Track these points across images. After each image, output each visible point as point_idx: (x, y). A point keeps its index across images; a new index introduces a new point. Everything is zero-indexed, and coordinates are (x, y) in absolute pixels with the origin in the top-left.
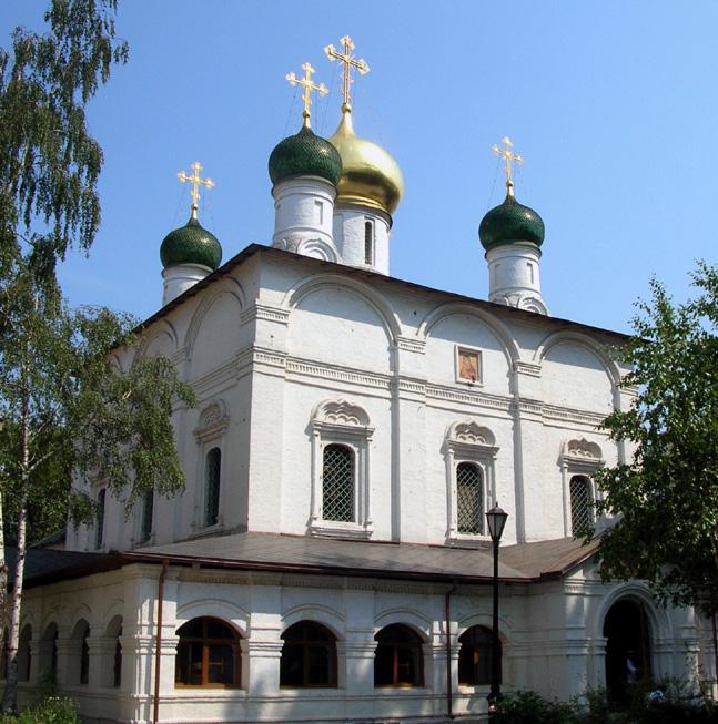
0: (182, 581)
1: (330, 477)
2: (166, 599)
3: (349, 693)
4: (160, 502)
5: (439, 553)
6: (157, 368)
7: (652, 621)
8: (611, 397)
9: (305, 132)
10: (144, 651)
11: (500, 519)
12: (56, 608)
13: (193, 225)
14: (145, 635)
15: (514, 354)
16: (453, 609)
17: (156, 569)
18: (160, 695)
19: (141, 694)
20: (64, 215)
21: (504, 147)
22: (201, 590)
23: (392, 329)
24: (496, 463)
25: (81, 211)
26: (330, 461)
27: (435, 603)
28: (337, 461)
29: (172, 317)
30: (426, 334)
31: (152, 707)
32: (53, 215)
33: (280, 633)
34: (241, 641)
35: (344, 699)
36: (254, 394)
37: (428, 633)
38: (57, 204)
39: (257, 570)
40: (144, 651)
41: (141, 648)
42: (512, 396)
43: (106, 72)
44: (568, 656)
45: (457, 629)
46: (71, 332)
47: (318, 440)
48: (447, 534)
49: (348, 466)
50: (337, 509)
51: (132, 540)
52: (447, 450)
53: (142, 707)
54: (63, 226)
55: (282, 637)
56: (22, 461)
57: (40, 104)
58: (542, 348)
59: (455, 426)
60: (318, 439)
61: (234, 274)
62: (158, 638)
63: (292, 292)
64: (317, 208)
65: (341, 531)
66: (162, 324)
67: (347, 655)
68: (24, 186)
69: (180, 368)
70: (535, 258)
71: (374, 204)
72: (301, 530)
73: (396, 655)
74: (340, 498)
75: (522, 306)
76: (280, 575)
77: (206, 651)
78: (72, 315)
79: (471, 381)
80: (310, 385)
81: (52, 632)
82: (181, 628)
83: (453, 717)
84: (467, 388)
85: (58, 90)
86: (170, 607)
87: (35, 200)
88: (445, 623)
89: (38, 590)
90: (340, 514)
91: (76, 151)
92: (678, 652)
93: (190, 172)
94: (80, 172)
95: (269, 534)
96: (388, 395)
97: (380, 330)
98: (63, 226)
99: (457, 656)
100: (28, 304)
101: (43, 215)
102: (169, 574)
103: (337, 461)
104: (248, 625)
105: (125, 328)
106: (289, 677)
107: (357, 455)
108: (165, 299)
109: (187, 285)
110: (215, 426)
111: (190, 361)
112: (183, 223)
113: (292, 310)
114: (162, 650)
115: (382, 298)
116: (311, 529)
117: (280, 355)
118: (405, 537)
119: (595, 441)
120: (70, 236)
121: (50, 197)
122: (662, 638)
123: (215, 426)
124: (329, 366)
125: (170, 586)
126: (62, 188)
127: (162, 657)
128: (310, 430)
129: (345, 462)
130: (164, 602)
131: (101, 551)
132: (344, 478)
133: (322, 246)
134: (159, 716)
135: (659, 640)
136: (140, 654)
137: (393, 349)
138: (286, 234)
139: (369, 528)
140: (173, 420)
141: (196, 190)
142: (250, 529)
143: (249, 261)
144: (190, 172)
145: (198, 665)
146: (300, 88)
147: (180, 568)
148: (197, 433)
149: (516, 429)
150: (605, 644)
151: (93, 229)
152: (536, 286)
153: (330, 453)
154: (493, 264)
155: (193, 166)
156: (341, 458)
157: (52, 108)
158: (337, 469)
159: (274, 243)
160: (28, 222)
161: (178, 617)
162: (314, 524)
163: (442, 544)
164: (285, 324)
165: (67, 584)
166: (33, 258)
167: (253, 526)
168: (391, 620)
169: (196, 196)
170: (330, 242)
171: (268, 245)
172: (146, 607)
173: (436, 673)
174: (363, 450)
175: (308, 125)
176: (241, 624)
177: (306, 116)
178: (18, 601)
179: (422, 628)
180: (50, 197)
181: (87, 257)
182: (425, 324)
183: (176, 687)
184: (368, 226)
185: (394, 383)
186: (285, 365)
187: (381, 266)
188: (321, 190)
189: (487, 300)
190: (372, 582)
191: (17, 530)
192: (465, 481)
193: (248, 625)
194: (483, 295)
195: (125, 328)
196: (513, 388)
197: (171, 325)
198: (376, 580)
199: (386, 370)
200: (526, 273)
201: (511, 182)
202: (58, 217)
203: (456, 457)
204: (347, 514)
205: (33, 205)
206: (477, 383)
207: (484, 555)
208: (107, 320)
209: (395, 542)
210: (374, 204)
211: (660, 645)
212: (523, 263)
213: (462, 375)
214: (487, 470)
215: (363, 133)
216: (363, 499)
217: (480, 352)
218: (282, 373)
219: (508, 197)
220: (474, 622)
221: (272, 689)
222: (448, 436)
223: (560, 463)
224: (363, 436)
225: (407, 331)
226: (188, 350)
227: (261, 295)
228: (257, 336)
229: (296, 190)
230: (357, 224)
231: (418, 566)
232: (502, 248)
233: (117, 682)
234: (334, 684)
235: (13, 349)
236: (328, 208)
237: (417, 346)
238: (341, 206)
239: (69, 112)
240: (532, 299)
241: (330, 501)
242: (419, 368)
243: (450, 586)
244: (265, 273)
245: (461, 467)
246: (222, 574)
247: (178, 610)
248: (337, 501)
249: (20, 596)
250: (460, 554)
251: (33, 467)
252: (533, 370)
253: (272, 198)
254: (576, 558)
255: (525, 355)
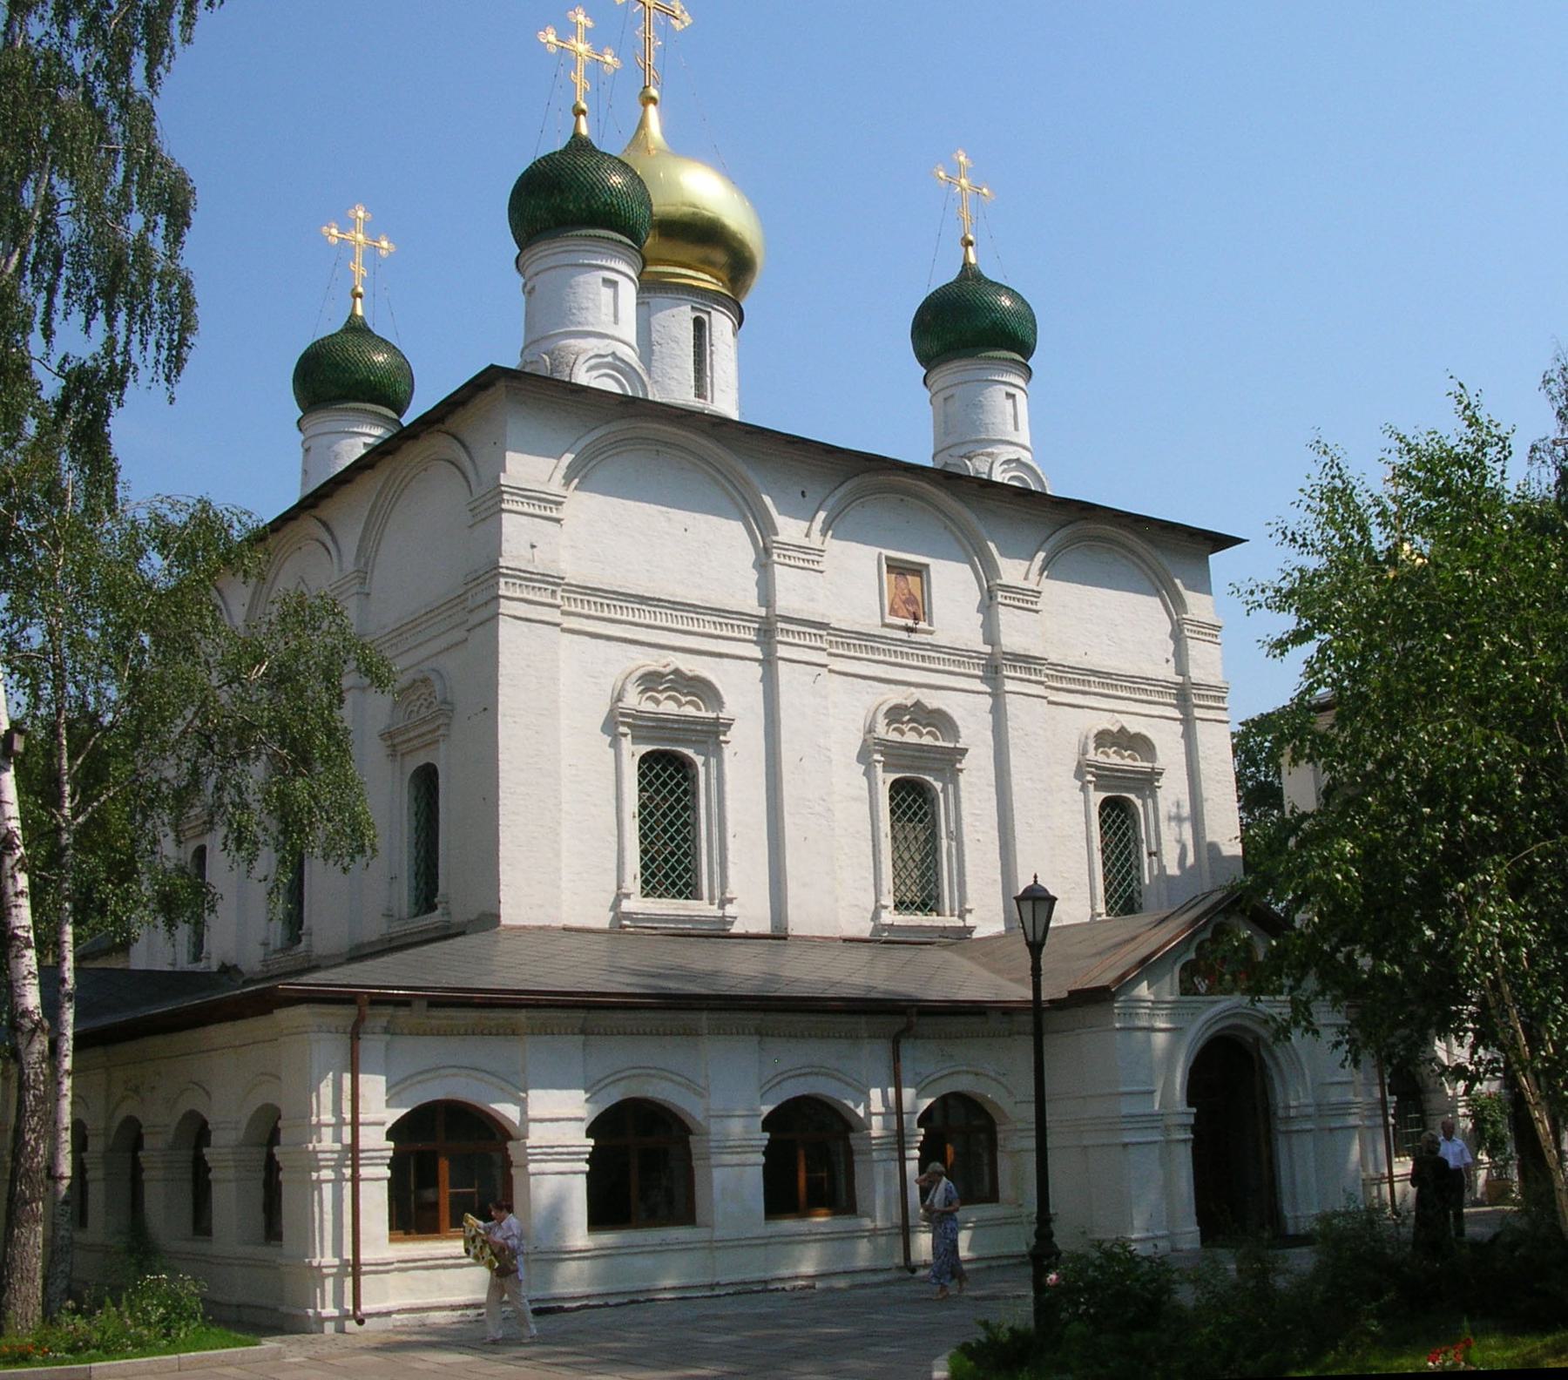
0: (393, 1034)
1: (651, 814)
2: (365, 1073)
3: (718, 1234)
4: (319, 875)
5: (864, 953)
6: (300, 615)
7: (1274, 1072)
8: (1171, 646)
9: (579, 145)
10: (327, 1174)
11: (1042, 908)
12: (136, 1090)
13: (356, 328)
14: (326, 1143)
15: (990, 569)
16: (906, 1065)
17: (346, 1014)
18: (365, 1256)
19: (326, 1258)
20: (122, 317)
21: (955, 170)
22: (428, 1051)
23: (761, 527)
24: (962, 778)
25: (156, 307)
26: (650, 783)
27: (873, 1055)
28: (664, 784)
29: (327, 510)
30: (824, 533)
31: (349, 1282)
32: (101, 316)
33: (584, 1126)
34: (510, 1145)
35: (712, 1246)
36: (502, 659)
37: (861, 1111)
38: (109, 293)
39: (537, 1006)
40: (327, 1174)
41: (318, 1169)
42: (988, 649)
43: (188, 24)
44: (1125, 1145)
45: (916, 1102)
46: (142, 551)
47: (626, 743)
48: (876, 915)
49: (685, 792)
50: (666, 876)
51: (265, 944)
52: (870, 753)
53: (329, 1284)
54: (121, 339)
55: (765, 1129)
56: (60, 807)
57: (64, 95)
58: (1041, 555)
59: (885, 708)
60: (626, 743)
61: (452, 423)
62: (354, 1148)
63: (569, 458)
64: (607, 292)
65: (677, 919)
66: (308, 525)
67: (713, 1162)
68: (40, 259)
69: (351, 610)
70: (1020, 382)
71: (706, 281)
72: (603, 920)
73: (801, 1153)
74: (672, 854)
75: (999, 476)
76: (582, 1014)
77: (444, 1166)
78: (143, 515)
79: (910, 623)
80: (609, 638)
81: (132, 1136)
82: (394, 1125)
83: (913, 1270)
84: (903, 635)
85: (99, 64)
86: (374, 1087)
87: (62, 287)
88: (891, 1091)
89: (97, 1054)
90: (673, 884)
91: (141, 186)
92: (1321, 1130)
93: (347, 224)
94: (150, 227)
95: (540, 928)
96: (757, 652)
97: (737, 528)
98: (121, 339)
99: (916, 1153)
100: (54, 493)
101: (78, 317)
102: (369, 1023)
103: (664, 784)
104: (524, 1112)
105: (236, 534)
106: (599, 1219)
107: (702, 770)
108: (304, 484)
109: (353, 449)
110: (424, 721)
111: (368, 594)
112: (336, 326)
113: (570, 492)
114: (364, 1172)
115: (742, 467)
116: (619, 915)
117: (553, 581)
118: (799, 923)
119: (1144, 732)
120: (136, 357)
121: (93, 281)
122: (1293, 1103)
123: (424, 721)
124: (643, 600)
125: (372, 1045)
126: (119, 264)
127: (362, 1185)
128: (611, 725)
129: (678, 785)
130: (362, 1077)
131: (201, 966)
132: (678, 816)
133: (619, 366)
134: (362, 1300)
135: (1288, 1107)
136: (320, 1182)
137: (764, 564)
138: (545, 345)
139: (730, 910)
140: (346, 715)
141: (359, 259)
142: (505, 920)
143: (483, 399)
144: (347, 224)
145: (429, 1195)
146: (565, 58)
147: (389, 1010)
148: (388, 735)
149: (1189, 737)
150: (1192, 1120)
151: (183, 342)
152: (1024, 437)
153: (651, 768)
154: (941, 396)
155: (351, 212)
156: (671, 777)
157: (89, 101)
158: (665, 799)
159: (526, 363)
160: (48, 333)
161: (389, 1104)
162: (627, 906)
163: (866, 934)
164: (558, 521)
165: (157, 1043)
166: (63, 405)
167: (511, 914)
168: (792, 1090)
169: (359, 270)
170: (631, 356)
171: (514, 367)
172: (326, 1089)
173: (880, 1187)
174: (713, 761)
175: (584, 130)
176: (509, 1111)
177: (579, 112)
178: (67, 1083)
179: (851, 1105)
180: (93, 281)
181: (172, 400)
182: (822, 515)
183: (391, 1240)
184: (699, 325)
185: (766, 631)
186: (558, 601)
187: (725, 402)
188: (613, 257)
189: (931, 464)
190: (754, 1019)
191: (59, 944)
192: (904, 813)
193: (524, 1112)
194: (923, 456)
195: (236, 534)
196: (990, 632)
197: (325, 524)
198: (761, 1015)
199: (751, 605)
200: (1003, 413)
201: (971, 237)
202: (111, 320)
203: (887, 767)
204: (687, 885)
205: (59, 301)
206: (922, 625)
207: (946, 954)
208: (206, 522)
209: (779, 936)
210: (706, 281)
211: (1289, 1118)
212: (998, 393)
213: (893, 612)
214: (944, 790)
215: (684, 145)
216: (716, 853)
217: (927, 566)
218: (554, 616)
219: (966, 265)
220: (946, 1087)
221: (579, 1235)
222: (870, 730)
223: (1079, 774)
224: (711, 734)
225: (789, 529)
226: (363, 575)
227: (508, 466)
228: (505, 546)
229: (551, 262)
230: (678, 320)
231: (833, 984)
232: (955, 365)
233: (272, 1229)
234: (686, 1216)
235: (25, 585)
236: (628, 291)
237: (808, 557)
238: (650, 287)
239: (124, 106)
240: (1018, 460)
241: (653, 860)
242: (812, 600)
243: (899, 1022)
244: (516, 423)
245: (896, 787)
246: (472, 1015)
247: (388, 1089)
248: (666, 861)
249: (68, 1073)
250: (904, 954)
251: (81, 819)
252: (1027, 599)
253: (517, 275)
254: (1144, 952)
255: (1012, 571)
